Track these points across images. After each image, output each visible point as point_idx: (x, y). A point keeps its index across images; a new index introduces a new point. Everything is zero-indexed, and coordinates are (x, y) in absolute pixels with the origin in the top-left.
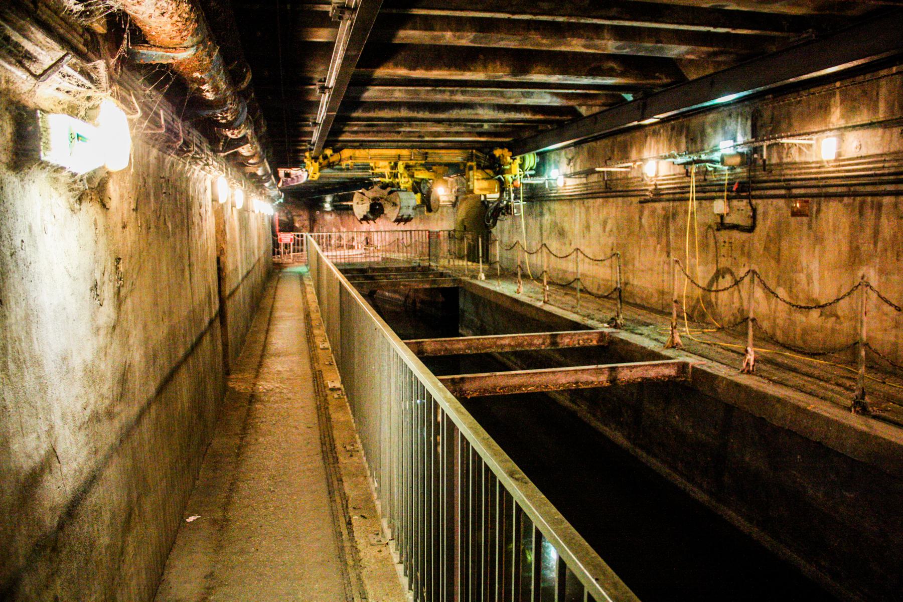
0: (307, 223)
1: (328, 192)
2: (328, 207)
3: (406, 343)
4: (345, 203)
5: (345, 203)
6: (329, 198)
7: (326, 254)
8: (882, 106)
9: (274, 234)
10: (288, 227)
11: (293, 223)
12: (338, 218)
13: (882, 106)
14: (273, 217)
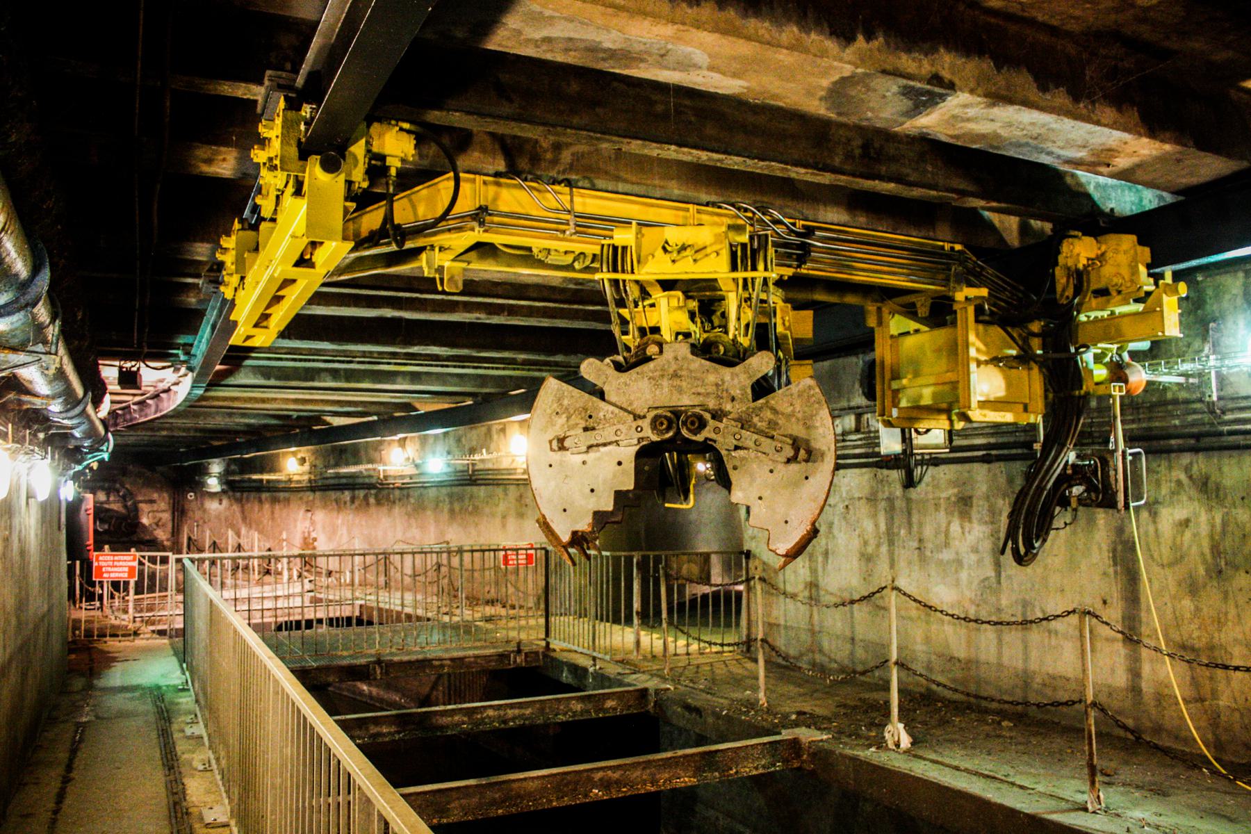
0: (166, 516)
1: (216, 453)
2: (213, 484)
3: (402, 795)
4: (255, 477)
5: (255, 477)
6: (216, 467)
7: (229, 594)
8: (257, 92)
9: (75, 549)
10: (123, 532)
11: (137, 517)
12: (236, 508)
13: (257, 92)
14: (74, 508)
